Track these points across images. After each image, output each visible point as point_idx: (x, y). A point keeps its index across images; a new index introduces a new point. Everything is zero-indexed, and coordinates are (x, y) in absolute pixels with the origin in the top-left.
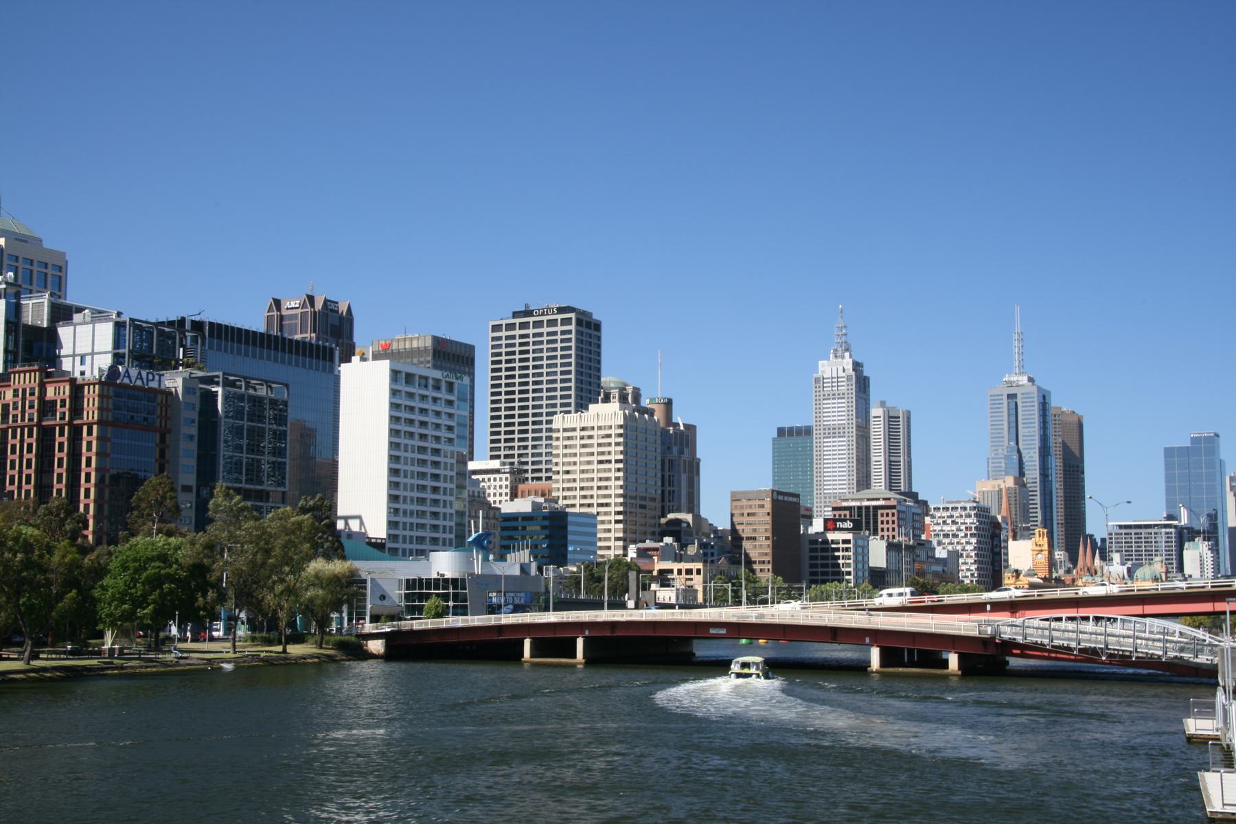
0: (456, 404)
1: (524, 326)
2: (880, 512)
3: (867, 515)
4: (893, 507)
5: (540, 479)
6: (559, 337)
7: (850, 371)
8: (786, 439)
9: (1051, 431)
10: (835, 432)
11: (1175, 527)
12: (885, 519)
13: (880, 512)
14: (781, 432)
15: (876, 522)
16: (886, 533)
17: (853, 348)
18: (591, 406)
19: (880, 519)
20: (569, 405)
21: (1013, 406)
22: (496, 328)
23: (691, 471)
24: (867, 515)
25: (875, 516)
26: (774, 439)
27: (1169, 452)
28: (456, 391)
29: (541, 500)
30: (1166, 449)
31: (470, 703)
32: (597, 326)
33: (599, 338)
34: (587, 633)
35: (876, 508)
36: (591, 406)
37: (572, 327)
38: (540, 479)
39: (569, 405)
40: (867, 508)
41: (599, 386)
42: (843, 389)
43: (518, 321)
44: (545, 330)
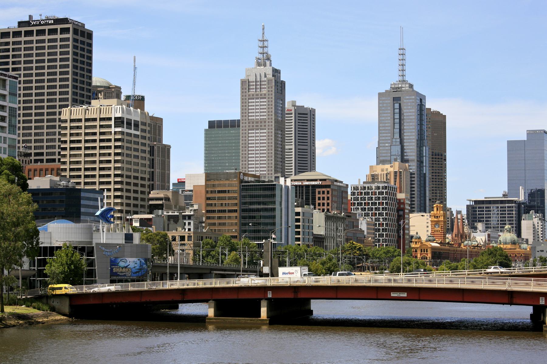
0: (8, 98)
1: (29, 33)
2: (317, 190)
3: (307, 193)
4: (329, 186)
5: (42, 161)
6: (23, 46)
7: (270, 76)
8: (216, 131)
9: (425, 127)
10: (258, 125)
11: (515, 202)
12: (321, 196)
13: (317, 190)
14: (212, 124)
15: (314, 199)
16: (325, 207)
17: (272, 59)
18: (93, 102)
19: (317, 196)
20: (67, 100)
21: (397, 106)
22: (391, 84)
23: (163, 156)
24: (307, 193)
25: (314, 193)
26: (206, 130)
27: (512, 146)
28: (8, 87)
29: (57, 179)
30: (510, 143)
31: (385, 360)
32: (90, 35)
33: (90, 45)
34: (270, 295)
35: (314, 186)
36: (93, 102)
37: (70, 35)
38: (54, 160)
39: (67, 100)
40: (307, 186)
41: (90, 84)
42: (264, 91)
43: (23, 29)
44: (35, 38)
